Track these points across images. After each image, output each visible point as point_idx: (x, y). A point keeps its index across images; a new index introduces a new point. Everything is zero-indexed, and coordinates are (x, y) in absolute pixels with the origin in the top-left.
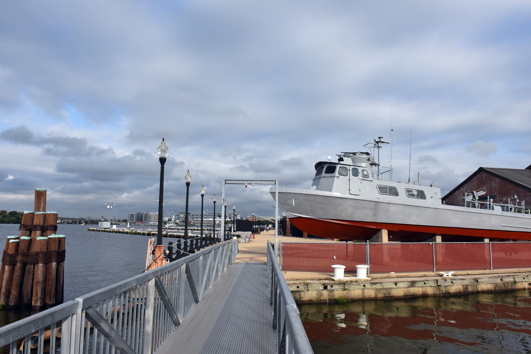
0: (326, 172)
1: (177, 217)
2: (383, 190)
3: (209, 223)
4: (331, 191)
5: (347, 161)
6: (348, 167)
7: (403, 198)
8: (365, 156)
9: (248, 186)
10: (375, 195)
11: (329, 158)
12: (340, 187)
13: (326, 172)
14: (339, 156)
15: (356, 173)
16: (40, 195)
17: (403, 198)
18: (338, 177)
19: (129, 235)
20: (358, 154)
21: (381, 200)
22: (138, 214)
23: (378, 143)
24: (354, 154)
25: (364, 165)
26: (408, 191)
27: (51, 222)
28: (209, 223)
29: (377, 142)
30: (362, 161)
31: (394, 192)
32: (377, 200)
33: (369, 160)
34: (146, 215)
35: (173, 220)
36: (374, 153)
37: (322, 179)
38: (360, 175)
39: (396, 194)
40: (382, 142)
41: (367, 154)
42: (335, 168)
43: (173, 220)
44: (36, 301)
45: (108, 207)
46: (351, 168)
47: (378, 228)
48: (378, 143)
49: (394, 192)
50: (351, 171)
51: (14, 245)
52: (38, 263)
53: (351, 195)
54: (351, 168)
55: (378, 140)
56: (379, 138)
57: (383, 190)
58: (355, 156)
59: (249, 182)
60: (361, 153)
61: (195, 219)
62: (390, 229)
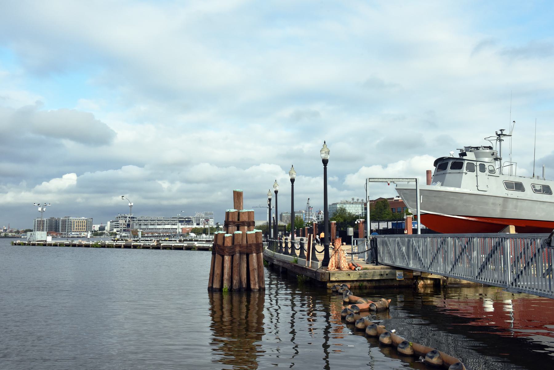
0: (451, 168)
1: (114, 224)
2: (509, 185)
3: (166, 232)
4: (460, 187)
5: (470, 156)
6: (475, 163)
7: (529, 193)
8: (488, 151)
9: (391, 184)
10: (504, 192)
11: (452, 153)
12: (468, 183)
13: (451, 168)
14: (461, 150)
15: (483, 168)
16: (238, 196)
17: (529, 193)
18: (466, 173)
19: (91, 248)
20: (481, 149)
21: (509, 196)
22: (51, 220)
23: (500, 136)
24: (477, 148)
25: (486, 159)
26: (534, 187)
27: (244, 218)
28: (166, 232)
29: (499, 135)
30: (486, 155)
31: (519, 187)
32: (506, 196)
33: (493, 154)
34: (64, 222)
35: (108, 228)
36: (495, 145)
37: (447, 175)
38: (487, 172)
39: (523, 190)
40: (504, 135)
41: (490, 148)
42: (462, 164)
43: (108, 228)
44: (255, 284)
45: (40, 209)
46: (478, 163)
47: (505, 223)
48: (500, 136)
49: (519, 187)
50: (478, 167)
51: (230, 238)
52: (252, 253)
53: (475, 189)
54: (478, 163)
55: (499, 133)
56: (501, 130)
57: (509, 185)
58: (478, 151)
59: (391, 180)
60: (484, 147)
61: (143, 227)
62: (518, 225)
